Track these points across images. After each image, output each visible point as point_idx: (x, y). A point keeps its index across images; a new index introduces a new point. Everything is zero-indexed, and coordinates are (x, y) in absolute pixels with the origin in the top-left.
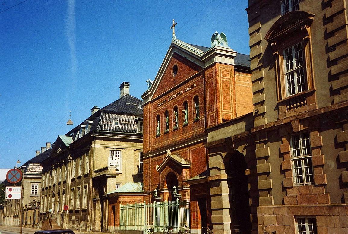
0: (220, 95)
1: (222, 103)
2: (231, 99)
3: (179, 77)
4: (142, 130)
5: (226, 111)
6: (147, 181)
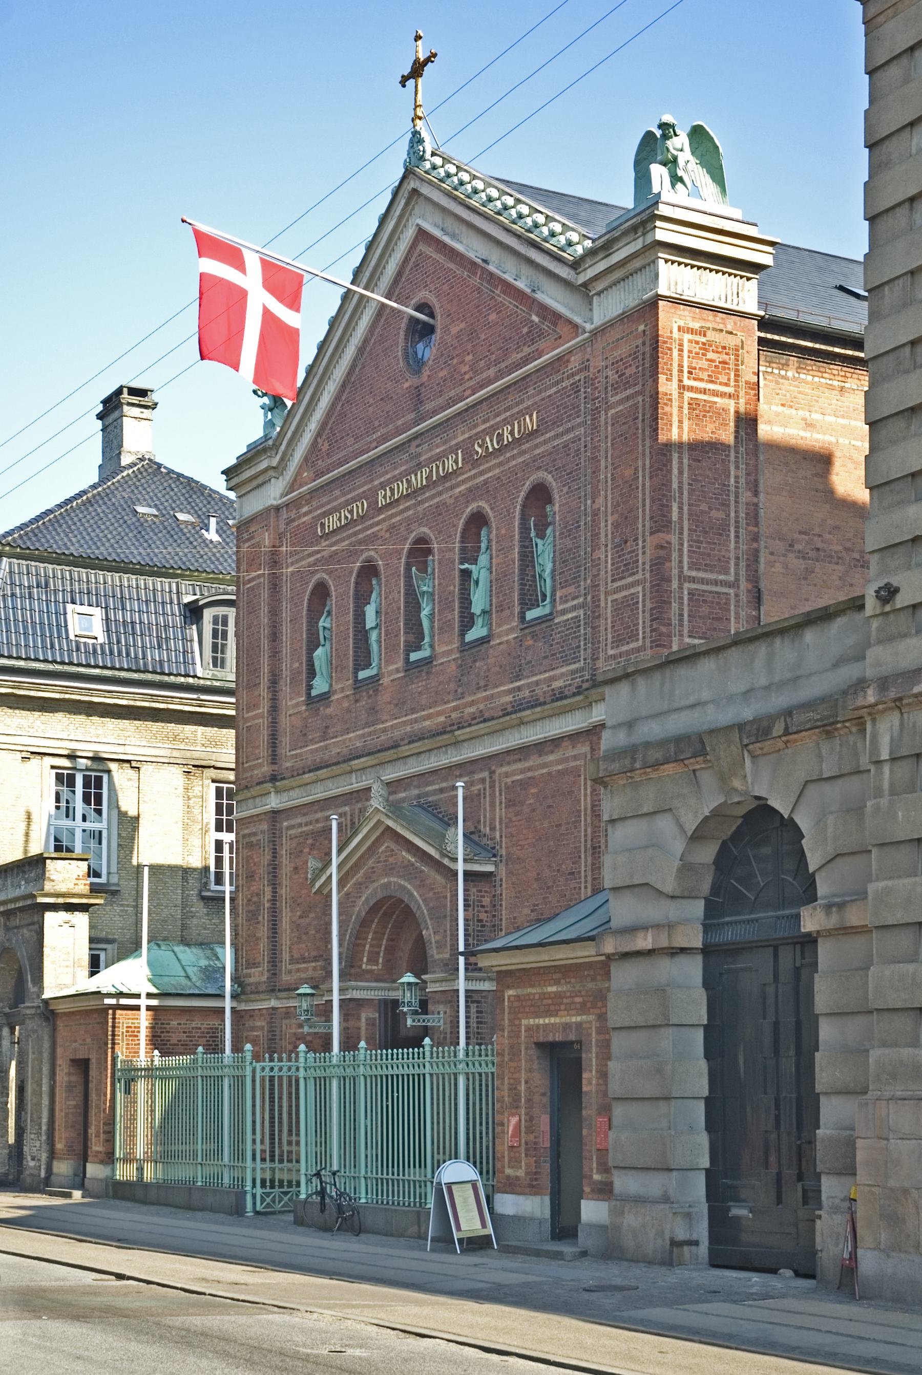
0: (675, 486)
1: (686, 533)
2: (732, 508)
3: (441, 374)
4: (223, 660)
5: (701, 575)
6: (258, 939)
